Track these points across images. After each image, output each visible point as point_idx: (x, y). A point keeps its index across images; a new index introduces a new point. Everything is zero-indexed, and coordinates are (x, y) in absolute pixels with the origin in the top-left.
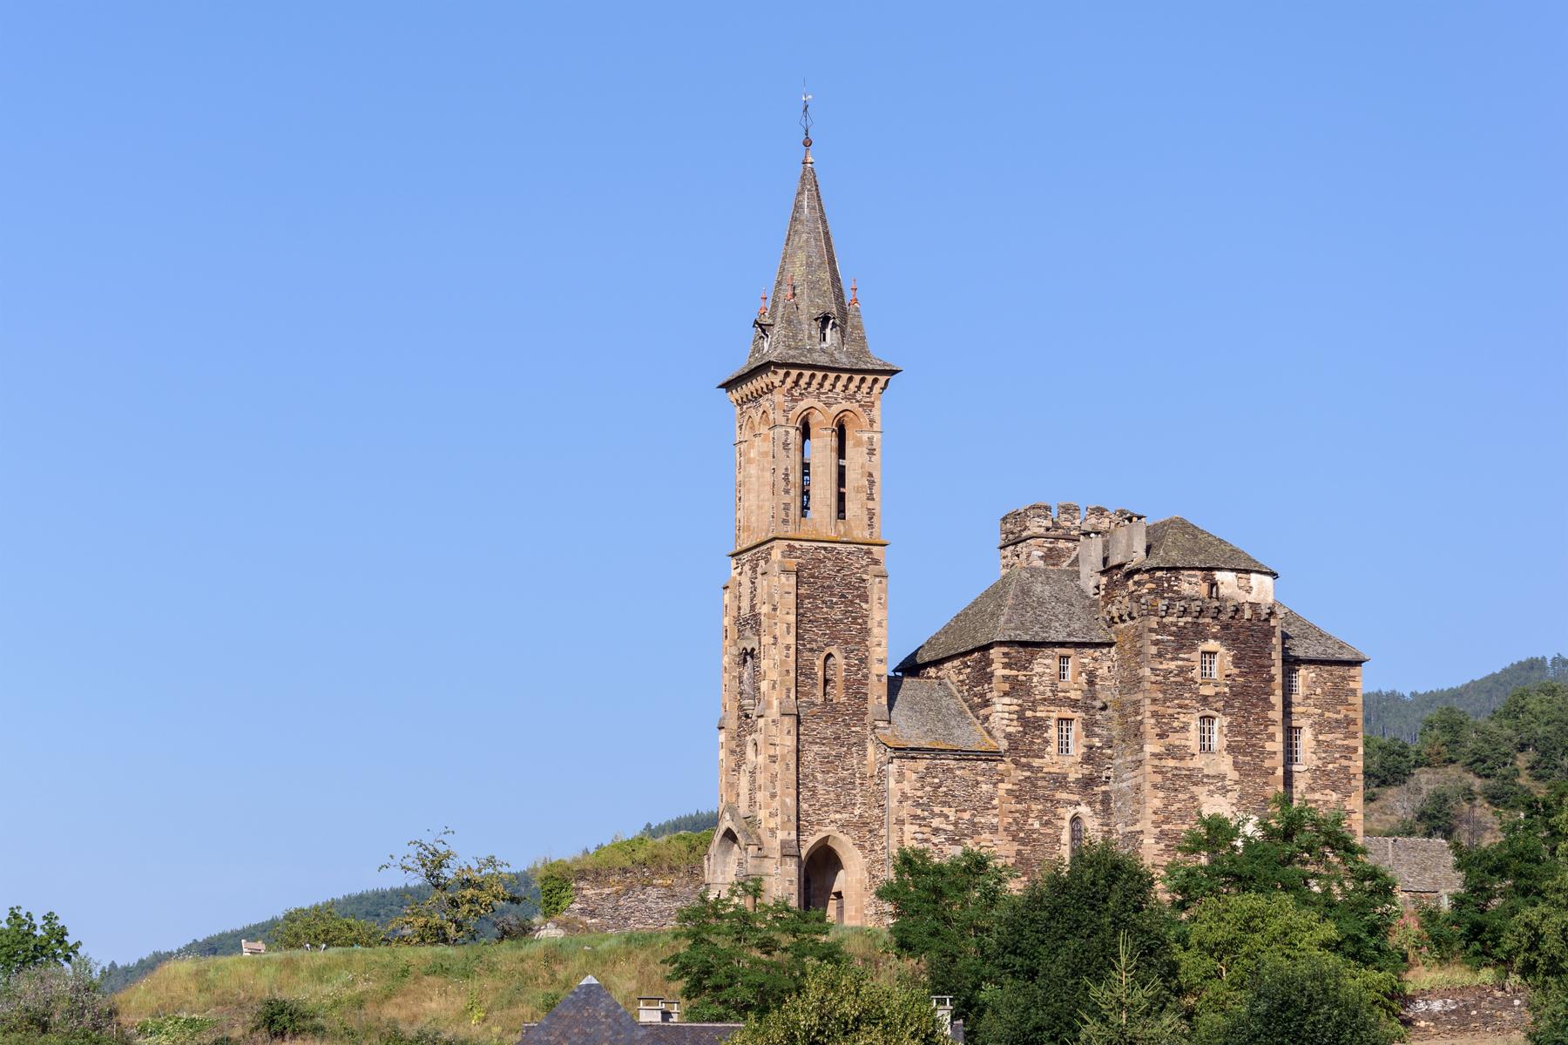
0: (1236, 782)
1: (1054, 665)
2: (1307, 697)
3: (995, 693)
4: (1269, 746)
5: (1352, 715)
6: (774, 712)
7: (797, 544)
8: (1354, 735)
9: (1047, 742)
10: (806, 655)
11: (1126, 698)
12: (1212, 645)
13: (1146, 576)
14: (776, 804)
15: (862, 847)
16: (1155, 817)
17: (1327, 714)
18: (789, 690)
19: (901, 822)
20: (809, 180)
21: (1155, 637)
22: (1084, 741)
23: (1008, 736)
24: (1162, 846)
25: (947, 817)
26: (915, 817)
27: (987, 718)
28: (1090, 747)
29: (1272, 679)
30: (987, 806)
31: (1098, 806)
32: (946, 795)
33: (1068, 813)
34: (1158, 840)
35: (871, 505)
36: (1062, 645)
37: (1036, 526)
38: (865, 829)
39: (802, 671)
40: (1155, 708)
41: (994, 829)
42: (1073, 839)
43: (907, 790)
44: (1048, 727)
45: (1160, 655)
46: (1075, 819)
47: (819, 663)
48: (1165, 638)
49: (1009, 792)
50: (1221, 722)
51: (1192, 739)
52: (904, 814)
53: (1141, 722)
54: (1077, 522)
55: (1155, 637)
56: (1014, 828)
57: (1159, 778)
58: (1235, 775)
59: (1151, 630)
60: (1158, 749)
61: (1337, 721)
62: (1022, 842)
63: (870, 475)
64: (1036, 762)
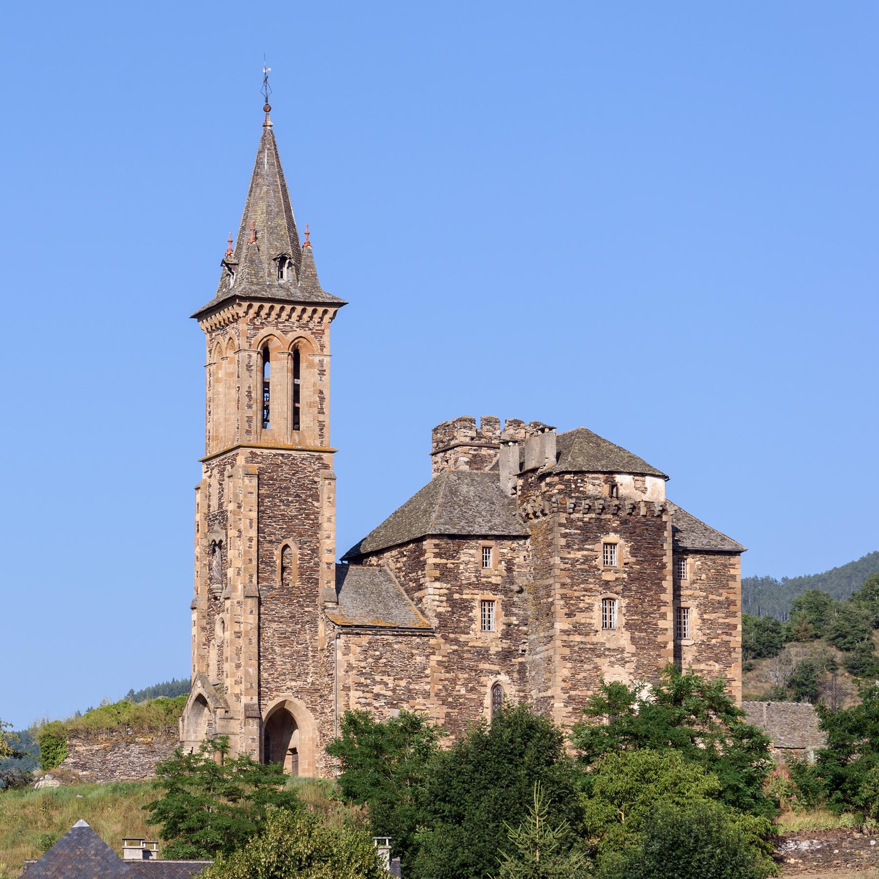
0: (633, 655)
1: (478, 554)
2: (694, 582)
3: (427, 579)
4: (662, 624)
6: (239, 595)
7: (258, 451)
8: (734, 615)
9: (471, 620)
10: (266, 546)
12: (612, 537)
13: (556, 479)
14: (240, 673)
15: (314, 710)
16: (564, 685)
17: (711, 597)
18: (251, 576)
19: (347, 689)
20: (269, 140)
21: (564, 530)
22: (503, 619)
23: (439, 615)
24: (570, 709)
25: (386, 684)
26: (359, 684)
27: (420, 600)
29: (664, 566)
30: (420, 675)
31: (516, 675)
32: (385, 665)
33: (490, 681)
34: (567, 704)
35: (321, 418)
36: (485, 537)
39: (263, 560)
40: (564, 591)
41: (426, 695)
42: (494, 703)
44: (472, 607)
45: (568, 546)
46: (496, 686)
47: (277, 552)
48: (573, 531)
49: (439, 663)
50: (621, 603)
51: (596, 618)
52: (350, 682)
53: (552, 603)
54: (498, 433)
55: (564, 530)
56: (443, 694)
57: (567, 651)
58: (632, 649)
59: (561, 525)
61: (719, 602)
62: (451, 706)
63: (321, 392)
64: (463, 638)
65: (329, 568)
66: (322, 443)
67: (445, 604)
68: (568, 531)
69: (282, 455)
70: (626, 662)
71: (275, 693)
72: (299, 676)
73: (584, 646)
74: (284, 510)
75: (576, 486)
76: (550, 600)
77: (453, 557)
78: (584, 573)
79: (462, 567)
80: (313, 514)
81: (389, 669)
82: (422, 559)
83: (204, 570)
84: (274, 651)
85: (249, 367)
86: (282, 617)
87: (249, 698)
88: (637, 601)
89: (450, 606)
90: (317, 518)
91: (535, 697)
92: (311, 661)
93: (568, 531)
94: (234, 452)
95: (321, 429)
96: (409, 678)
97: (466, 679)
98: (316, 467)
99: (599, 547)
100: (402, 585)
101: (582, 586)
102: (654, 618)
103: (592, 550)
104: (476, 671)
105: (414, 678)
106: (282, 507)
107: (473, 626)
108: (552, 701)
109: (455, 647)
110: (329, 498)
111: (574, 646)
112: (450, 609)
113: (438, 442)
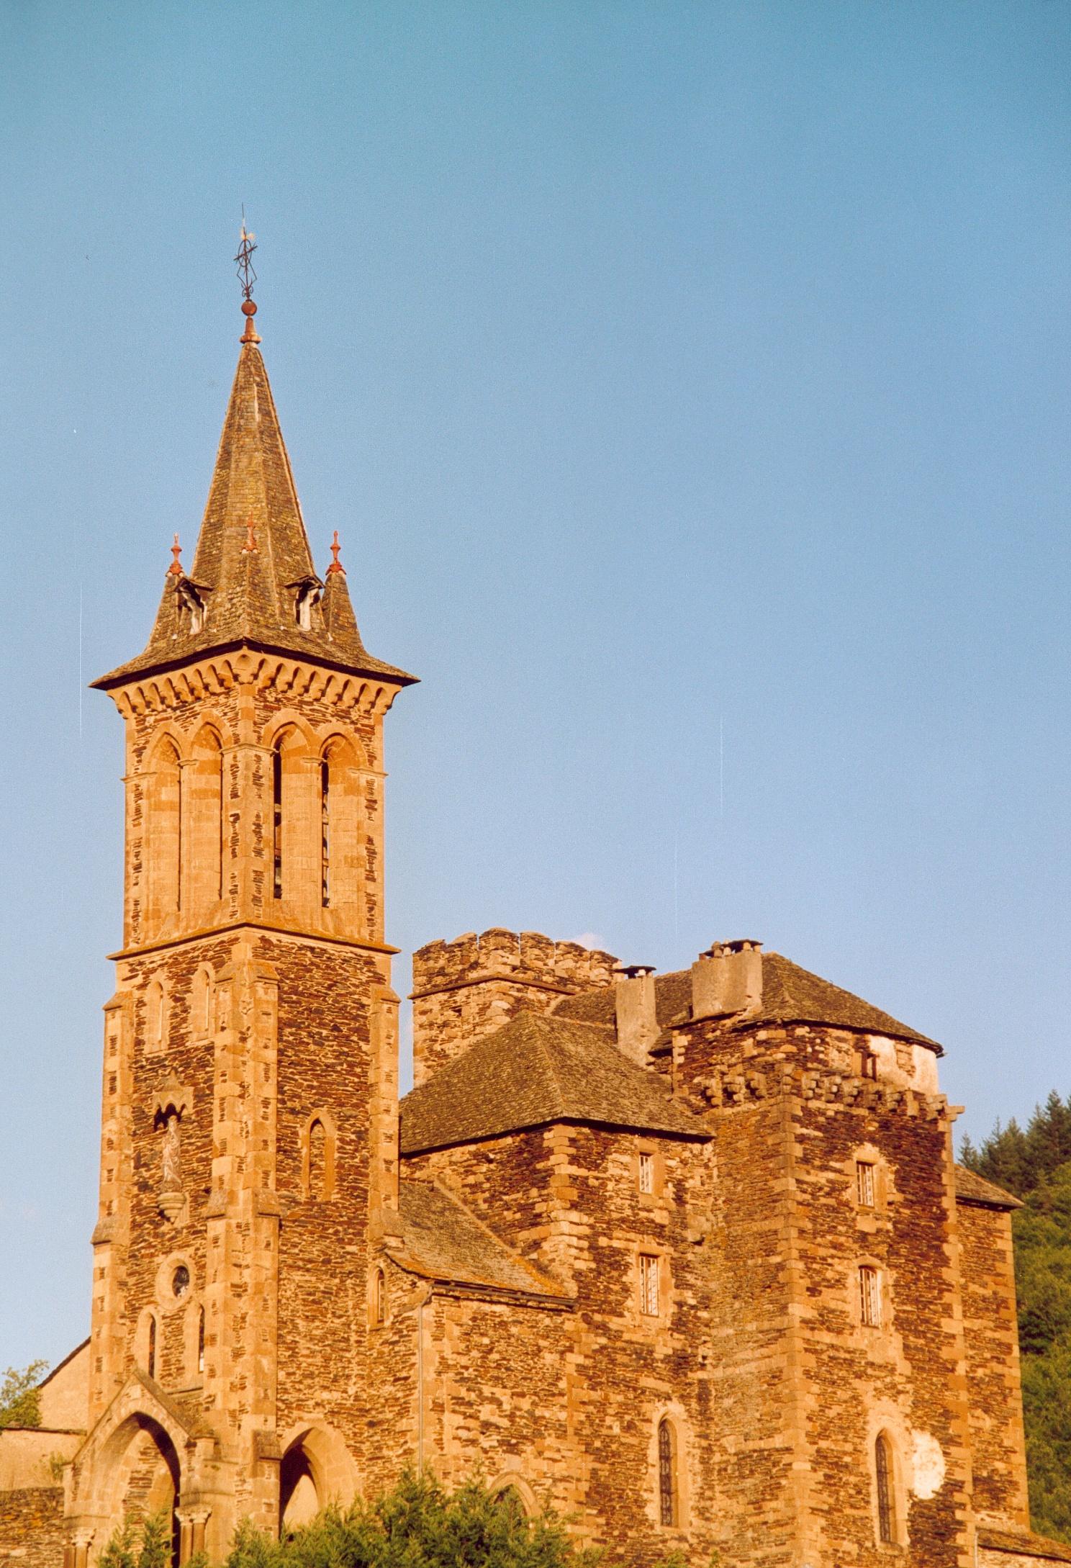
3: (557, 1203)
5: (1003, 1293)
6: (242, 1209)
7: (273, 937)
11: (737, 1230)
13: (782, 1033)
14: (240, 1368)
15: (357, 1452)
16: (809, 1426)
18: (266, 1174)
20: (251, 365)
23: (577, 1275)
24: (820, 1476)
25: (500, 1404)
26: (459, 1401)
27: (536, 1245)
28: (680, 1304)
30: (550, 1394)
31: (694, 1405)
35: (371, 888)
36: (645, 1133)
37: (497, 963)
38: (364, 1420)
43: (448, 1354)
44: (627, 1266)
45: (805, 1160)
49: (581, 1369)
52: (443, 1395)
53: (780, 1267)
54: (551, 962)
57: (811, 1361)
58: (904, 1367)
59: (795, 1119)
60: (811, 1314)
61: (984, 1299)
62: (599, 1455)
63: (370, 841)
64: (614, 1323)
65: (388, 1170)
66: (371, 935)
67: (586, 1255)
68: (804, 1131)
69: (312, 949)
70: (899, 1392)
71: (295, 1413)
72: (335, 1380)
73: (837, 1354)
74: (314, 1053)
75: (814, 1051)
76: (775, 1259)
77: (597, 1166)
78: (831, 1211)
79: (610, 1186)
80: (360, 1064)
81: (503, 1373)
82: (540, 1166)
83: (125, 1166)
84: (295, 1326)
85: (257, 777)
86: (310, 1261)
87: (262, 1418)
88: (910, 1276)
89: (594, 1260)
90: (365, 1074)
91: (732, 1450)
92: (354, 1352)
93: (804, 1131)
94: (225, 937)
95: (371, 909)
96: (535, 1394)
97: (620, 1405)
98: (364, 979)
99: (849, 1166)
100: (482, 1217)
101: (829, 1238)
102: (935, 1312)
103: (839, 1171)
104: (635, 1389)
105: (542, 1394)
106: (312, 1047)
107: (629, 1303)
108: (786, 1458)
109: (603, 1341)
110: (389, 1037)
111: (822, 1352)
112: (593, 1265)
113: (430, 975)
